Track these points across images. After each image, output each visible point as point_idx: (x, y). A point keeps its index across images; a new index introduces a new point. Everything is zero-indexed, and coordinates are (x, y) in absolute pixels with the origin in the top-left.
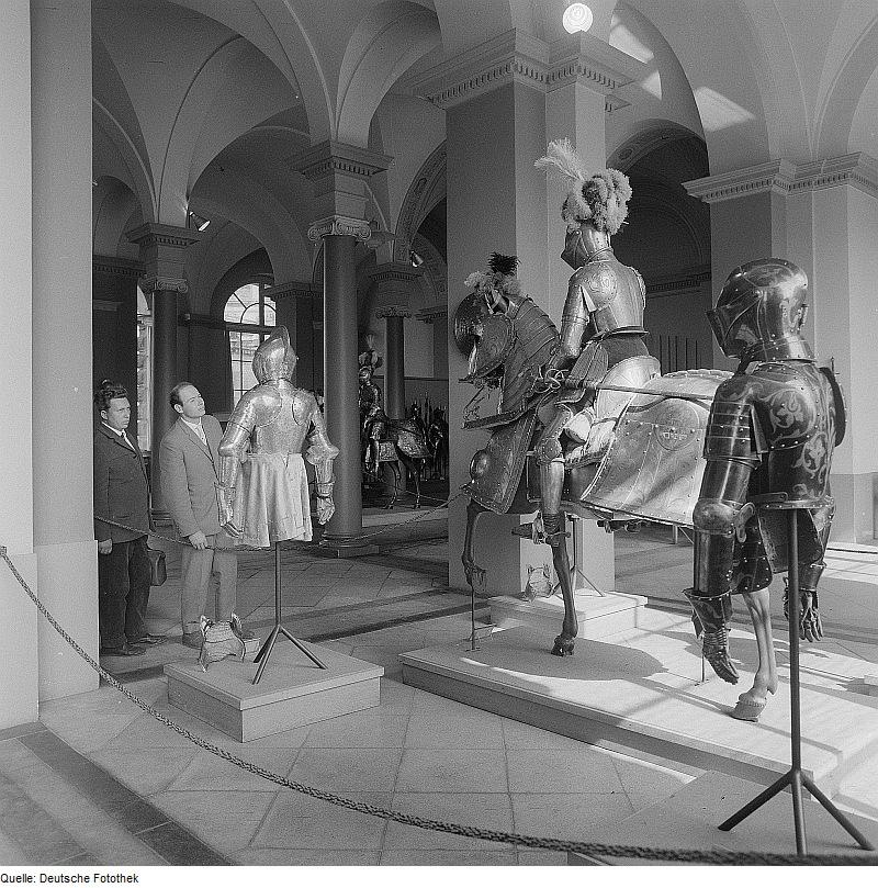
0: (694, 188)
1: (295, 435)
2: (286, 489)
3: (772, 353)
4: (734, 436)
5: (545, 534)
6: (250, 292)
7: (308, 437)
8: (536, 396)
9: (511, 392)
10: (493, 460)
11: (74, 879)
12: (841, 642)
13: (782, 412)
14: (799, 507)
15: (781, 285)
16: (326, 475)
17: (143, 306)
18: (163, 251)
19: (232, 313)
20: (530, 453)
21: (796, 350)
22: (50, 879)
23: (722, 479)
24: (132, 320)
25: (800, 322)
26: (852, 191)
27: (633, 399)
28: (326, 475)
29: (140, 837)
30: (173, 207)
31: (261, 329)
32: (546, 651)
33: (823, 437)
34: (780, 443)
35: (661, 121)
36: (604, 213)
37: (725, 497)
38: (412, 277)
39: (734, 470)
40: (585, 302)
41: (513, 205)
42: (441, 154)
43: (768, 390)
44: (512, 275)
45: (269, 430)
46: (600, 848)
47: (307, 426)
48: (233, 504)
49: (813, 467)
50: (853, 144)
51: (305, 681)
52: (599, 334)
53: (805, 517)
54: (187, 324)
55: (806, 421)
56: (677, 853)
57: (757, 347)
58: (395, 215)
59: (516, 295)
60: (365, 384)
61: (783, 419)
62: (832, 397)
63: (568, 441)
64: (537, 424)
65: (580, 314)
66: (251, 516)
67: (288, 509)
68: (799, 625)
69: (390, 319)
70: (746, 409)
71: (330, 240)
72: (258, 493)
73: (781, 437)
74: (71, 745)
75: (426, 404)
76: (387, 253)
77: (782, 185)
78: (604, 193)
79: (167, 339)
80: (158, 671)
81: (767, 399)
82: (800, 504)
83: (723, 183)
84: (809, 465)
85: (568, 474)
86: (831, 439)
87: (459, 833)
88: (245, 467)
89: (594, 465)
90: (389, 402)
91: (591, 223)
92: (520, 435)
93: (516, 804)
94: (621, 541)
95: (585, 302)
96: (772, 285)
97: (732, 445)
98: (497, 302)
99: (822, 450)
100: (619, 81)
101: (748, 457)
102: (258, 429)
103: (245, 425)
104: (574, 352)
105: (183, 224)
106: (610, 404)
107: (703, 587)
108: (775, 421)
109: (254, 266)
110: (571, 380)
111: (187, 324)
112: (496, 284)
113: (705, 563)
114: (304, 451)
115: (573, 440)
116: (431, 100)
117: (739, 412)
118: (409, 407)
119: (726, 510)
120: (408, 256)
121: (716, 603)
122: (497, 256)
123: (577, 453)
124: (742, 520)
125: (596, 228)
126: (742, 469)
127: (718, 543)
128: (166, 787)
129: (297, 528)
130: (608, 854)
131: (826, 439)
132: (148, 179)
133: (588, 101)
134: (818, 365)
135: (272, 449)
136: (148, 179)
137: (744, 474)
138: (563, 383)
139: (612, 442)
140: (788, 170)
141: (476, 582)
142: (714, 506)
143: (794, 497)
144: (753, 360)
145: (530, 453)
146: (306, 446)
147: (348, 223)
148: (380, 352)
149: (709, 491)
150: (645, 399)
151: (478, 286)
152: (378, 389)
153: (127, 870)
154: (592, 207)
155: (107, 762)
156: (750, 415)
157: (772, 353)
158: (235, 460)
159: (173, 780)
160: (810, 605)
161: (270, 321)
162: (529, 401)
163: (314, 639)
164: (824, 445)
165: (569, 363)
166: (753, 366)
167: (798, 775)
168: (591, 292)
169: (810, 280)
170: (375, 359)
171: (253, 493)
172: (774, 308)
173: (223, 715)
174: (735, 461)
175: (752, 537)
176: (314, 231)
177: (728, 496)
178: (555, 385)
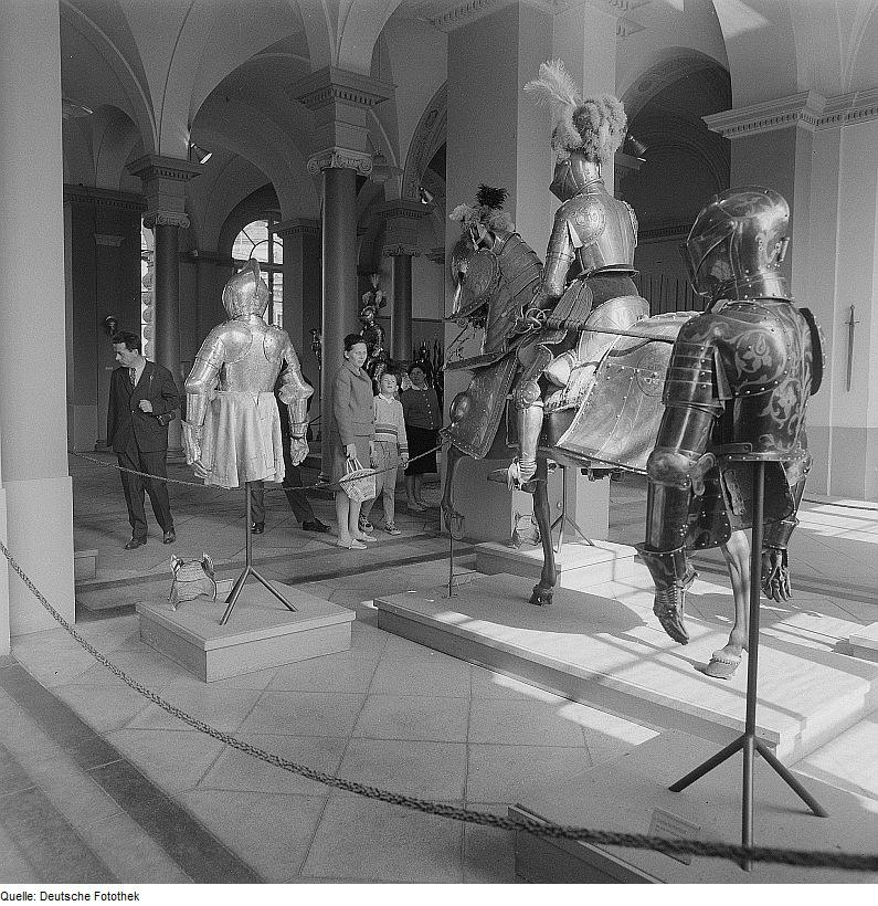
0: (715, 122)
1: (267, 374)
3: (744, 290)
4: (695, 382)
6: (257, 230)
7: (280, 376)
8: (517, 337)
9: (494, 333)
10: (472, 404)
14: (765, 459)
15: (759, 216)
16: (300, 416)
17: (147, 240)
18: (164, 184)
19: (240, 251)
20: (509, 397)
21: (772, 286)
23: (680, 426)
24: (137, 255)
25: (779, 257)
27: (616, 342)
29: (90, 773)
30: (174, 138)
31: (270, 267)
32: (525, 599)
33: (794, 384)
35: (686, 49)
36: (595, 143)
38: (422, 215)
39: (694, 417)
42: (445, 87)
45: (239, 367)
46: (491, 819)
47: (279, 363)
48: (201, 443)
49: (782, 416)
52: (584, 272)
53: (775, 472)
54: (194, 260)
55: (774, 366)
56: (565, 830)
57: (729, 283)
58: (404, 150)
59: (503, 231)
60: (369, 324)
61: (749, 363)
62: (809, 341)
63: (548, 385)
64: (519, 366)
65: (565, 252)
66: (219, 455)
67: (258, 446)
68: (766, 580)
69: (398, 258)
71: (330, 173)
73: (746, 383)
74: (39, 679)
75: (435, 346)
76: (396, 188)
78: (596, 121)
79: (169, 277)
81: (732, 341)
82: (767, 456)
83: (743, 118)
85: (546, 421)
86: (805, 389)
88: (214, 405)
89: (572, 411)
90: (395, 340)
91: (581, 152)
92: (501, 376)
96: (749, 215)
97: (693, 390)
98: (482, 237)
99: (793, 398)
101: (709, 404)
102: (227, 366)
104: (557, 291)
105: (184, 155)
106: (595, 348)
107: (656, 541)
108: (740, 365)
109: (260, 203)
112: (482, 218)
113: (657, 517)
114: (277, 390)
115: (552, 384)
116: (432, 22)
117: (702, 356)
118: (417, 350)
119: (682, 460)
120: (417, 192)
121: (668, 561)
123: (556, 397)
124: (700, 472)
125: (586, 158)
128: (123, 725)
131: (798, 386)
132: (150, 113)
134: (798, 306)
135: (242, 387)
136: (150, 113)
137: (704, 423)
138: (544, 324)
139: (591, 386)
140: (817, 103)
141: (454, 527)
143: (760, 448)
145: (509, 397)
146: (278, 386)
147: (350, 155)
148: (386, 292)
149: (665, 438)
150: (631, 342)
152: (382, 329)
154: (582, 135)
155: (70, 697)
156: (713, 358)
157: (744, 290)
158: (203, 397)
161: (278, 260)
162: (511, 341)
163: (296, 581)
165: (553, 302)
166: (721, 304)
167: (751, 740)
169: (791, 212)
170: (378, 299)
171: (222, 432)
172: (749, 244)
173: (187, 655)
174: (696, 408)
175: (711, 489)
176: (313, 164)
177: (686, 445)
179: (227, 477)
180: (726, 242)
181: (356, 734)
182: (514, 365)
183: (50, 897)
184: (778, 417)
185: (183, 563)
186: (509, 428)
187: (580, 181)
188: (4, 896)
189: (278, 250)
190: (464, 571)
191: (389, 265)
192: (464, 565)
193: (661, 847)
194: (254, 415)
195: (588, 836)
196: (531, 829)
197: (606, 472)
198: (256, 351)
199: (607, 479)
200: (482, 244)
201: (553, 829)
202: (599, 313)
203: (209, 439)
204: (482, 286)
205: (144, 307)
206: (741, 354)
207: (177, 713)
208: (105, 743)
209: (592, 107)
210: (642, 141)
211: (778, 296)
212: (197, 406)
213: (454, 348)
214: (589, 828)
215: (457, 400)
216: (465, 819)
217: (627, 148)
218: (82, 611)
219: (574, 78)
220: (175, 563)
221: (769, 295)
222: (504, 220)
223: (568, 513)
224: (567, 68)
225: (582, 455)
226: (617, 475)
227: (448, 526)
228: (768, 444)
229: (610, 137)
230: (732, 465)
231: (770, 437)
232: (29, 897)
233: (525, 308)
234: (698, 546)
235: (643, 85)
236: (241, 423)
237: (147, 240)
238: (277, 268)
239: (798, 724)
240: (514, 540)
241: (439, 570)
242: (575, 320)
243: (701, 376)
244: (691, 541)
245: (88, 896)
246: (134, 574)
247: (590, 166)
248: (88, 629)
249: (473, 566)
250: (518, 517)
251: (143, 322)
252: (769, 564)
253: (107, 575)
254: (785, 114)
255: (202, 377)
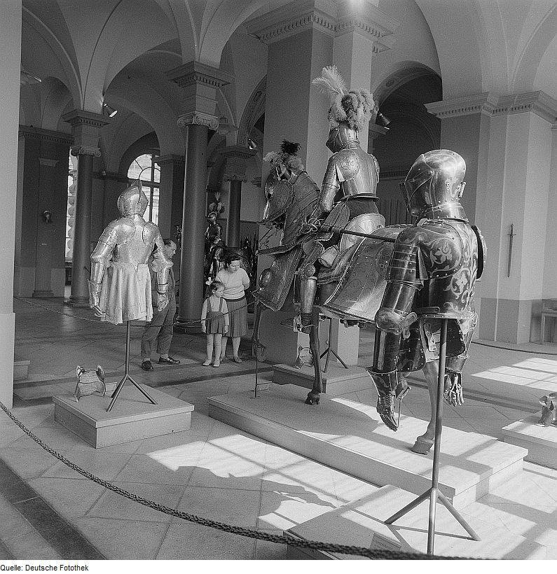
0: (431, 107)
1: (143, 250)
2: (135, 286)
4: (406, 268)
6: (145, 160)
8: (303, 236)
9: (289, 232)
10: (273, 275)
16: (163, 279)
17: (73, 163)
19: (133, 173)
23: (396, 296)
24: (66, 172)
26: (533, 119)
30: (93, 100)
31: (151, 184)
35: (414, 63)
37: (397, 308)
38: (252, 154)
39: (404, 290)
42: (265, 78)
43: (430, 238)
44: (295, 155)
46: (265, 536)
50: (537, 85)
54: (103, 178)
55: (454, 261)
58: (240, 113)
60: (212, 223)
61: (439, 258)
63: (319, 265)
64: (303, 254)
67: (136, 299)
71: (192, 127)
73: (436, 270)
75: (255, 239)
76: (233, 139)
77: (487, 110)
78: (355, 104)
80: (49, 400)
81: (429, 244)
82: (448, 315)
87: (186, 518)
88: (109, 271)
91: (345, 123)
92: (292, 259)
98: (283, 172)
102: (119, 246)
104: (328, 208)
105: (99, 111)
107: (380, 367)
108: (433, 259)
109: (147, 143)
111: (103, 178)
114: (150, 265)
119: (396, 316)
121: (386, 378)
122: (286, 142)
124: (407, 324)
125: (349, 127)
127: (391, 338)
128: (40, 475)
130: (269, 540)
132: (78, 83)
138: (319, 228)
140: (493, 100)
142: (388, 313)
143: (444, 310)
147: (206, 117)
148: (225, 203)
149: (386, 304)
151: (272, 161)
154: (347, 113)
156: (417, 254)
158: (102, 265)
160: (456, 382)
161: (157, 180)
162: (298, 238)
166: (423, 221)
168: (342, 169)
171: (113, 288)
173: (84, 431)
174: (406, 284)
176: (181, 121)
179: (116, 317)
180: (428, 183)
181: (190, 483)
182: (300, 253)
183: (32, 568)
184: (456, 292)
185: (84, 371)
186: (295, 291)
187: (344, 140)
188: (3, 568)
189: (157, 174)
190: (265, 381)
191: (227, 186)
192: (266, 378)
193: (366, 554)
194: (135, 280)
195: (322, 547)
196: (289, 542)
197: (355, 322)
198: (138, 237)
199: (356, 327)
200: (283, 177)
201: (302, 542)
202: (353, 223)
203: (105, 292)
204: (282, 202)
205: (69, 206)
206: (434, 252)
207: (74, 467)
208: (28, 487)
209: (353, 96)
210: (387, 117)
211: (458, 218)
212: (99, 272)
213: (263, 241)
214: (324, 542)
215: (264, 274)
216: (249, 536)
217: (378, 121)
218: (17, 400)
219: (343, 78)
220: (79, 371)
221: (452, 217)
222: (298, 163)
223: (332, 348)
224: (340, 72)
225: (339, 311)
226: (362, 324)
227: (255, 354)
228: (449, 308)
229: (364, 114)
230: (428, 320)
231: (451, 304)
232: (18, 568)
233: (308, 218)
234: (405, 370)
235: (389, 83)
236: (126, 282)
237: (73, 163)
238: (157, 185)
239: (476, 478)
240: (297, 363)
241: (248, 381)
242: (338, 227)
243: (409, 264)
244: (401, 367)
245: (56, 567)
246: (53, 377)
247: (351, 132)
248: (20, 412)
249: (273, 380)
250: (301, 349)
251: (68, 215)
252: (449, 382)
253: (36, 378)
254: (461, 108)
255: (101, 254)
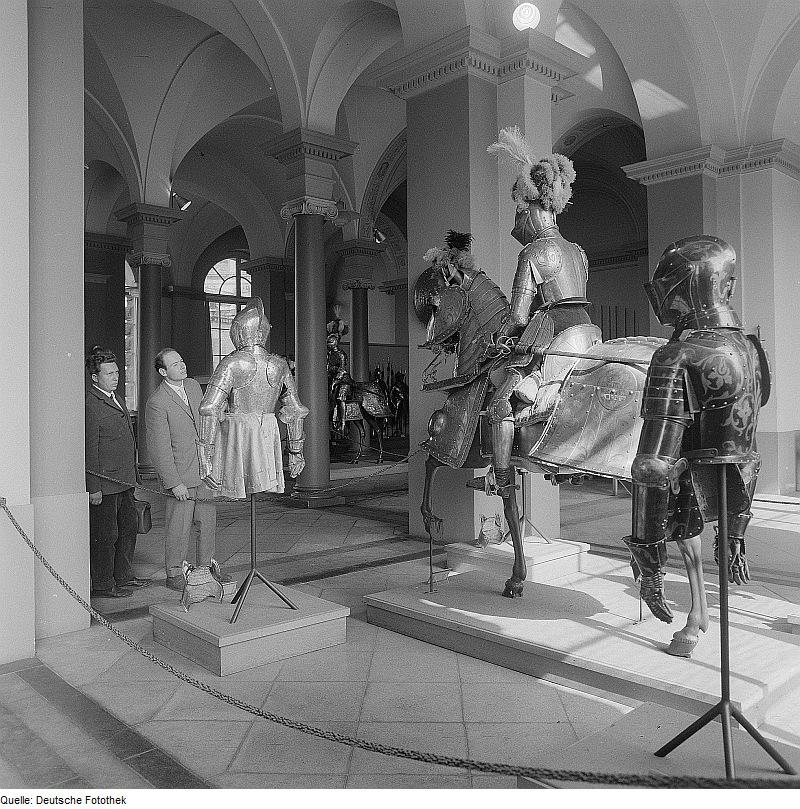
0: (632, 171)
1: (268, 397)
2: (261, 445)
3: (704, 321)
4: (669, 398)
5: (497, 487)
6: (228, 266)
7: (280, 398)
8: (488, 361)
9: (466, 357)
10: (449, 419)
11: (68, 801)
12: (766, 585)
13: (712, 376)
14: (728, 462)
15: (712, 260)
16: (297, 433)
17: (130, 278)
18: (149, 229)
19: (211, 285)
20: (483, 413)
21: (725, 319)
22: (46, 801)
23: (658, 436)
24: (121, 292)
25: (729, 294)
26: (776, 174)
27: (577, 364)
28: (297, 433)
29: (127, 762)
30: (157, 188)
31: (237, 300)
32: (498, 593)
33: (750, 398)
34: (710, 404)
35: (602, 110)
36: (550, 194)
37: (661, 453)
38: (376, 252)
39: (669, 428)
40: (533, 275)
41: (468, 187)
42: (402, 140)
43: (700, 355)
44: (467, 250)
45: (245, 392)
46: (547, 773)
47: (279, 388)
48: (212, 459)
49: (741, 425)
50: (777, 131)
51: (278, 621)
52: (546, 304)
53: (733, 471)
54: (170, 295)
55: (734, 384)
56: (617, 777)
57: (690, 316)
58: (359, 196)
59: (470, 269)
60: (332, 350)
61: (714, 382)
62: (758, 362)
63: (518, 402)
64: (489, 386)
65: (528, 286)
66: (229, 470)
67: (263, 464)
68: (728, 569)
69: (355, 291)
70: (680, 372)
71: (301, 218)
72: (235, 449)
73: (711, 398)
74: (65, 678)
75: (388, 368)
76: (353, 230)
77: (712, 169)
78: (550, 176)
79: (152, 309)
80: (144, 611)
81: (699, 364)
82: (729, 459)
83: (659, 167)
84: (737, 423)
85: (517, 432)
86: (757, 400)
87: (418, 759)
88: (223, 425)
89: (541, 424)
90: (354, 366)
91: (539, 203)
92: (474, 396)
93: (470, 733)
94: (566, 493)
95: (533, 275)
96: (704, 259)
97: (667, 405)
98: (453, 275)
99: (749, 410)
100: (564, 74)
101: (681, 416)
102: (235, 391)
103: (223, 387)
104: (523, 320)
105: (166, 204)
106: (556, 368)
107: (640, 534)
108: (706, 383)
109: (232, 242)
110: (521, 346)
111: (170, 295)
112: (452, 259)
113: (643, 513)
114: (277, 411)
115: (522, 401)
116: (393, 91)
117: (674, 376)
118: (372, 371)
119: (662, 465)
120: (372, 233)
121: (652, 549)
122: (453, 233)
123: (526, 413)
124: (676, 474)
125: (543, 207)
126: (676, 427)
127: (654, 495)
128: (151, 717)
129: (271, 481)
130: (554, 778)
131: (753, 400)
132: (135, 163)
133: (536, 92)
134: (745, 333)
135: (247, 409)
136: (135, 163)
137: (678, 432)
138: (513, 349)
139: (557, 402)
140: (718, 155)
141: (433, 530)
142: (651, 461)
143: (723, 453)
144: (687, 328)
145: (483, 413)
146: (279, 407)
147: (317, 203)
148: (346, 320)
149: (646, 447)
150: (588, 364)
151: (436, 260)
152: (344, 354)
153: (116, 793)
154: (539, 189)
155: (98, 694)
156: (684, 378)
157: (704, 321)
158: (215, 419)
159: (158, 711)
160: (738, 551)
161: (246, 292)
162: (482, 365)
163: (286, 583)
164: (751, 405)
165: (519, 331)
166: (686, 334)
167: (727, 706)
168: (538, 266)
169: (738, 255)
170: (341, 327)
171: (230, 449)
172: (705, 280)
173: (203, 652)
174: (670, 420)
175: (686, 489)
176: (286, 211)
177: (663, 452)
178: (506, 351)
